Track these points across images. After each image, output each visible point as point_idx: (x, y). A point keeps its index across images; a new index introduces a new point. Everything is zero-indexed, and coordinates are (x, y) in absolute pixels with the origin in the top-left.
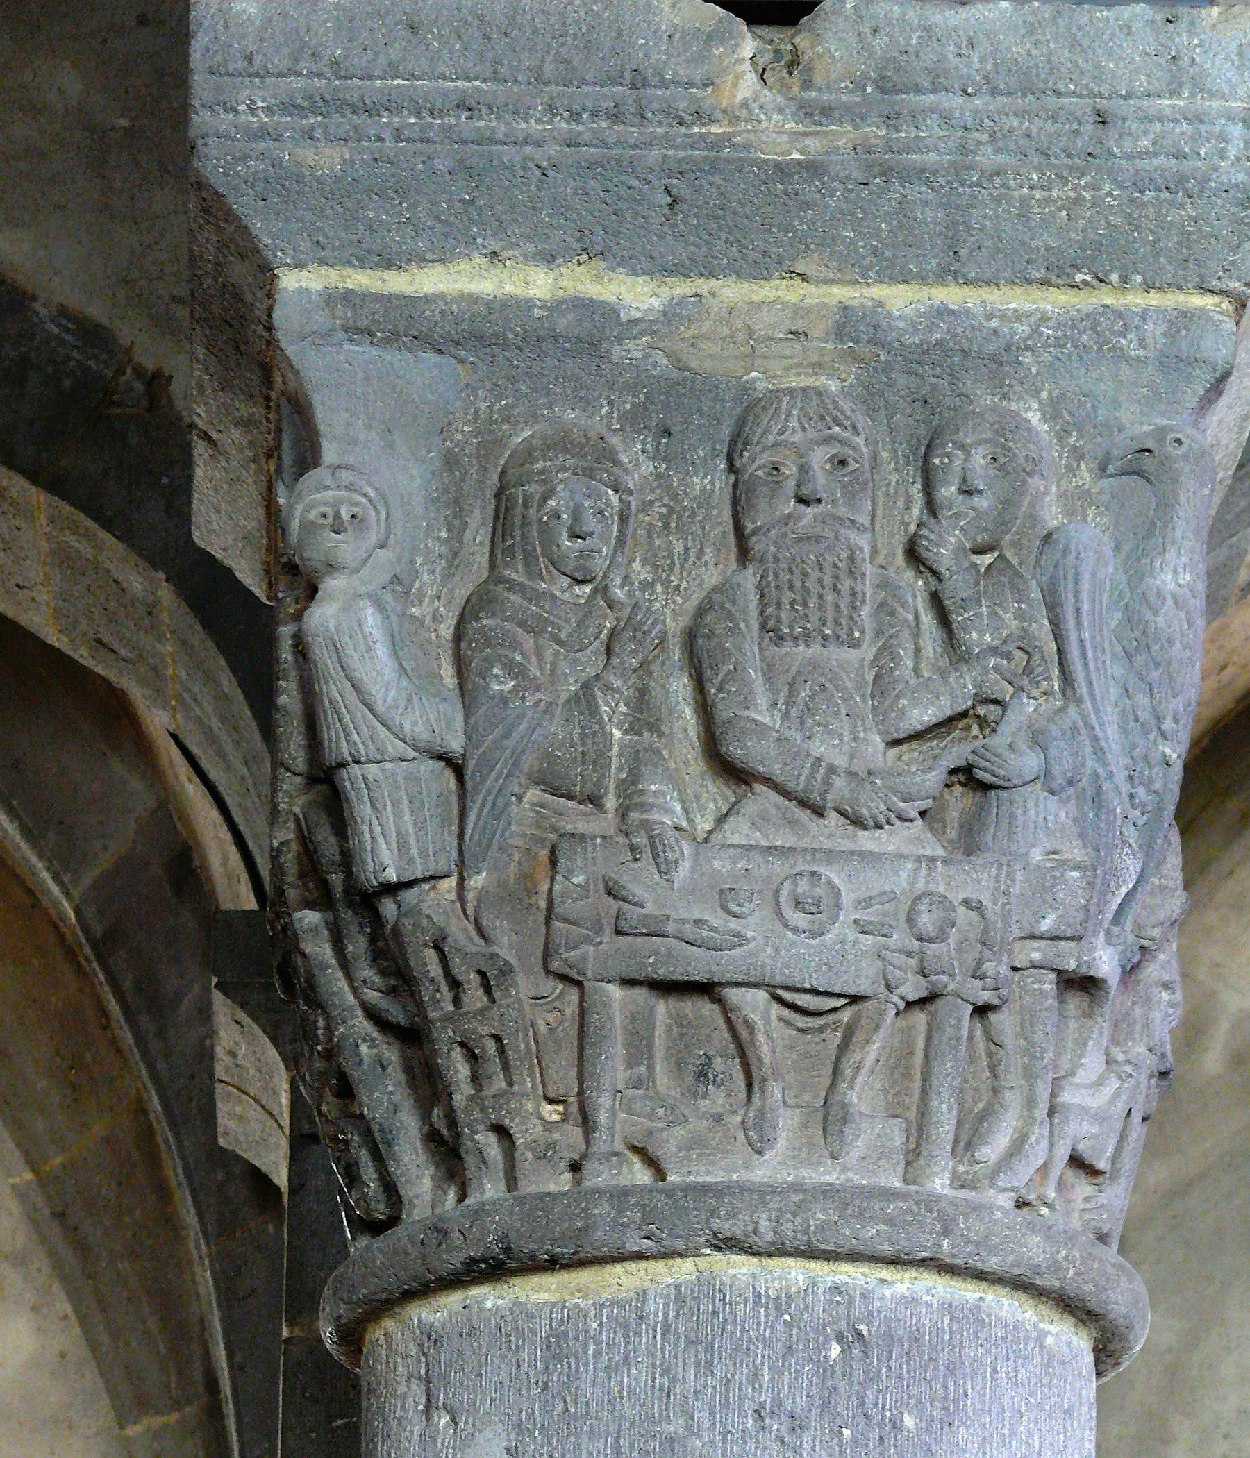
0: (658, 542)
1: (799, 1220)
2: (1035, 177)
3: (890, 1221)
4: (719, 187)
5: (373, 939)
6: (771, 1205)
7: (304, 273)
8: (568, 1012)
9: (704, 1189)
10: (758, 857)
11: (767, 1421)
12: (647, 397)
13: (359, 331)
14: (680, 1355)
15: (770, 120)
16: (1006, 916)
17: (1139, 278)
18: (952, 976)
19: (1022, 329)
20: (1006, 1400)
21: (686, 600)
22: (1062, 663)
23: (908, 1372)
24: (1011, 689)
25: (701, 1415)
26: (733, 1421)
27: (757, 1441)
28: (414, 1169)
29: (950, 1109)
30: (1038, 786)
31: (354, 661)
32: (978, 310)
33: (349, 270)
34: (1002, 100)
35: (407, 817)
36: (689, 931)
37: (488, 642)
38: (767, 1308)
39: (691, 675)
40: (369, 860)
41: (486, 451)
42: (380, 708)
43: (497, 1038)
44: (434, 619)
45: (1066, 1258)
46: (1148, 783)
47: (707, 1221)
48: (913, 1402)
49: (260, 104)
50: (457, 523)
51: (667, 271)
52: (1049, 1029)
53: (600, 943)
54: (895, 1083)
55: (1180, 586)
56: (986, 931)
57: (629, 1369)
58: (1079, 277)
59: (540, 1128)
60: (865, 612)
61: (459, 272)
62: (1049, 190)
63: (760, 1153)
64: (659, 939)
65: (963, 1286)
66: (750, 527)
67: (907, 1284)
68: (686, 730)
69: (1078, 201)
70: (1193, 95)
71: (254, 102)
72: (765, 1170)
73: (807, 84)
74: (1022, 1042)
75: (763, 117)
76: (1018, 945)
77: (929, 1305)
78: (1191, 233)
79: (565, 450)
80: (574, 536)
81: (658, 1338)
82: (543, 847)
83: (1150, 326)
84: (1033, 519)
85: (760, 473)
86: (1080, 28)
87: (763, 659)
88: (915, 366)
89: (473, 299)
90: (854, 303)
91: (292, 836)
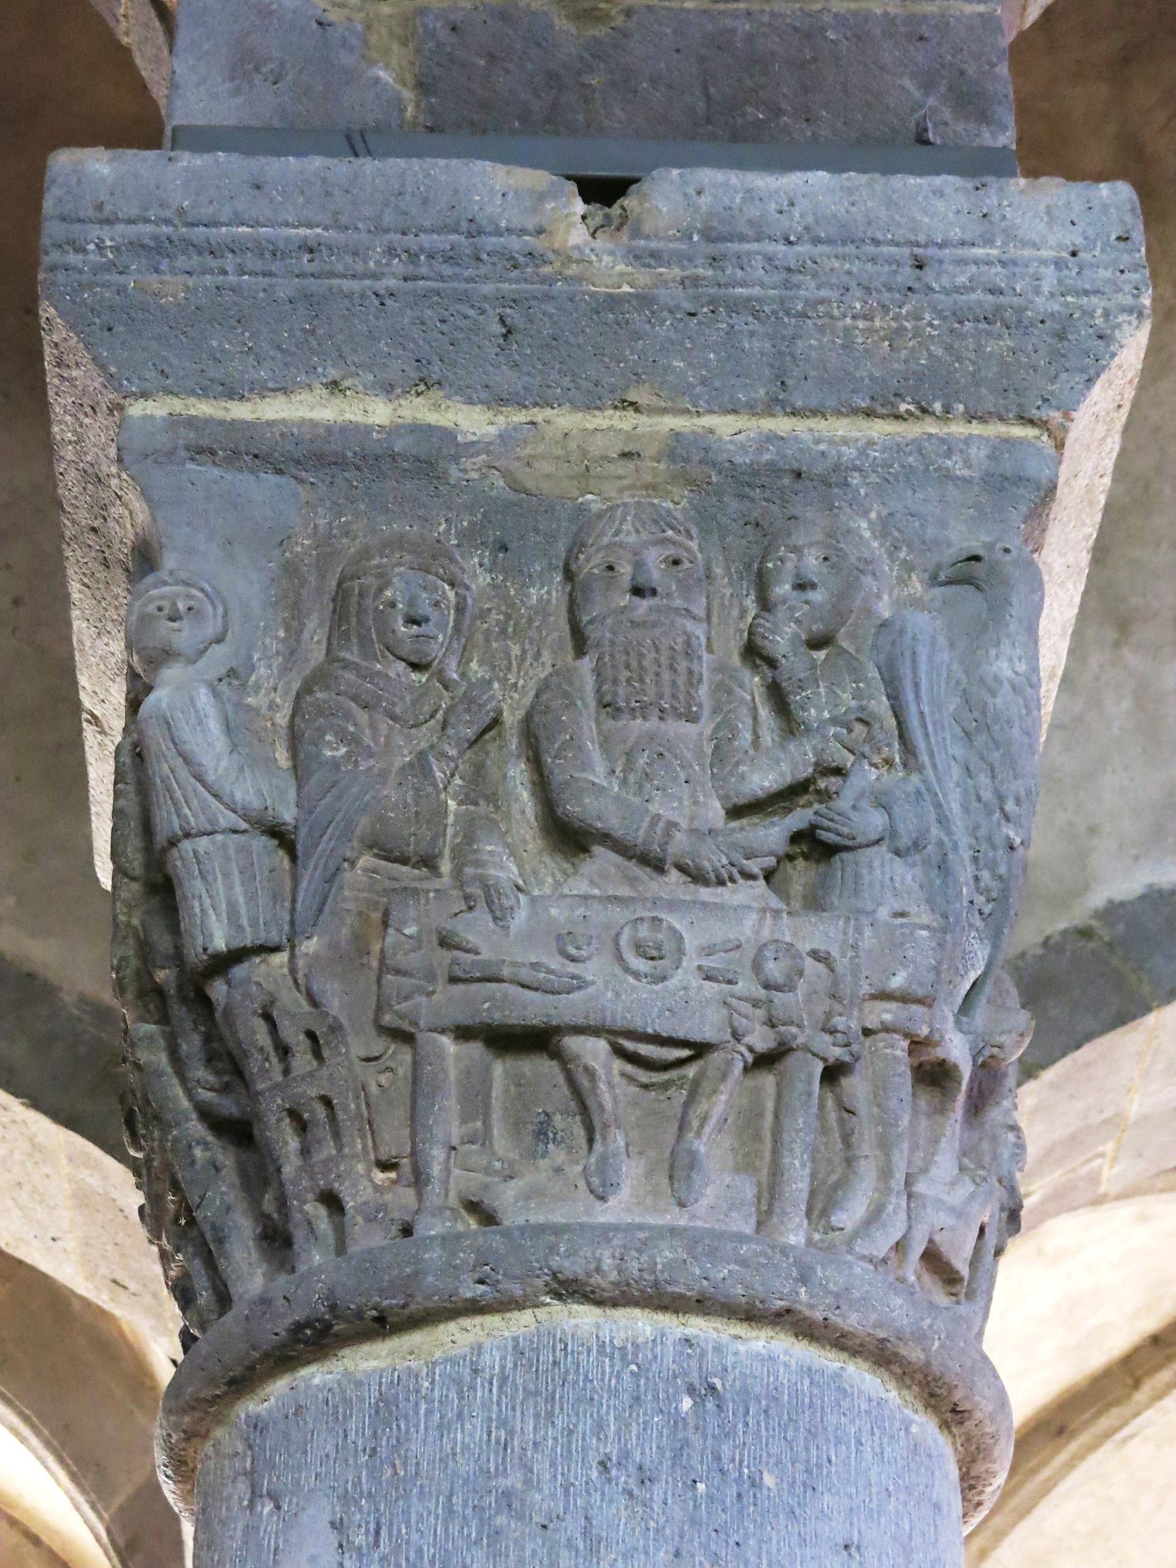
0: (495, 645)
1: (644, 1258)
2: (858, 305)
3: (743, 1263)
4: (551, 316)
5: (208, 1039)
6: (615, 1242)
7: (150, 403)
8: (401, 1071)
9: (543, 1229)
10: (597, 906)
11: (614, 1472)
12: (484, 515)
13: (200, 451)
14: (518, 1408)
15: (600, 261)
16: (855, 971)
17: (961, 407)
18: (800, 1026)
19: (849, 452)
20: (874, 1479)
21: (523, 695)
22: (902, 737)
23: (767, 1429)
24: (852, 758)
25: (541, 1466)
26: (576, 1473)
27: (603, 1493)
28: (245, 1268)
29: (803, 1166)
30: (883, 847)
31: (185, 732)
32: (806, 436)
33: (192, 400)
34: (821, 248)
35: (238, 889)
36: (525, 974)
37: (320, 712)
38: (612, 1358)
39: (528, 759)
40: (198, 933)
41: (323, 566)
42: (211, 777)
43: (327, 1102)
44: (270, 707)
45: (931, 1326)
46: (992, 866)
47: (546, 1260)
48: (772, 1461)
49: (108, 243)
50: (295, 624)
51: (502, 401)
52: (903, 1096)
53: (433, 992)
54: (744, 1144)
55: (1016, 673)
56: (835, 983)
57: (463, 1426)
58: (903, 407)
59: (370, 1190)
60: (703, 692)
61: (301, 402)
62: (872, 319)
63: (602, 1198)
64: (494, 986)
65: (823, 1353)
66: (585, 618)
67: (761, 1343)
68: (523, 812)
69: (900, 331)
70: (1005, 243)
71: (103, 241)
72: (609, 1213)
73: (636, 233)
74: (875, 1110)
75: (594, 258)
76: (868, 1005)
77: (786, 1365)
78: (1010, 364)
79: (401, 548)
80: (412, 621)
81: (495, 1390)
82: (376, 909)
83: (973, 451)
84: (868, 612)
85: (596, 571)
86: (894, 192)
87: (600, 733)
88: (747, 489)
89: (314, 424)
90: (686, 430)
91: (131, 953)
